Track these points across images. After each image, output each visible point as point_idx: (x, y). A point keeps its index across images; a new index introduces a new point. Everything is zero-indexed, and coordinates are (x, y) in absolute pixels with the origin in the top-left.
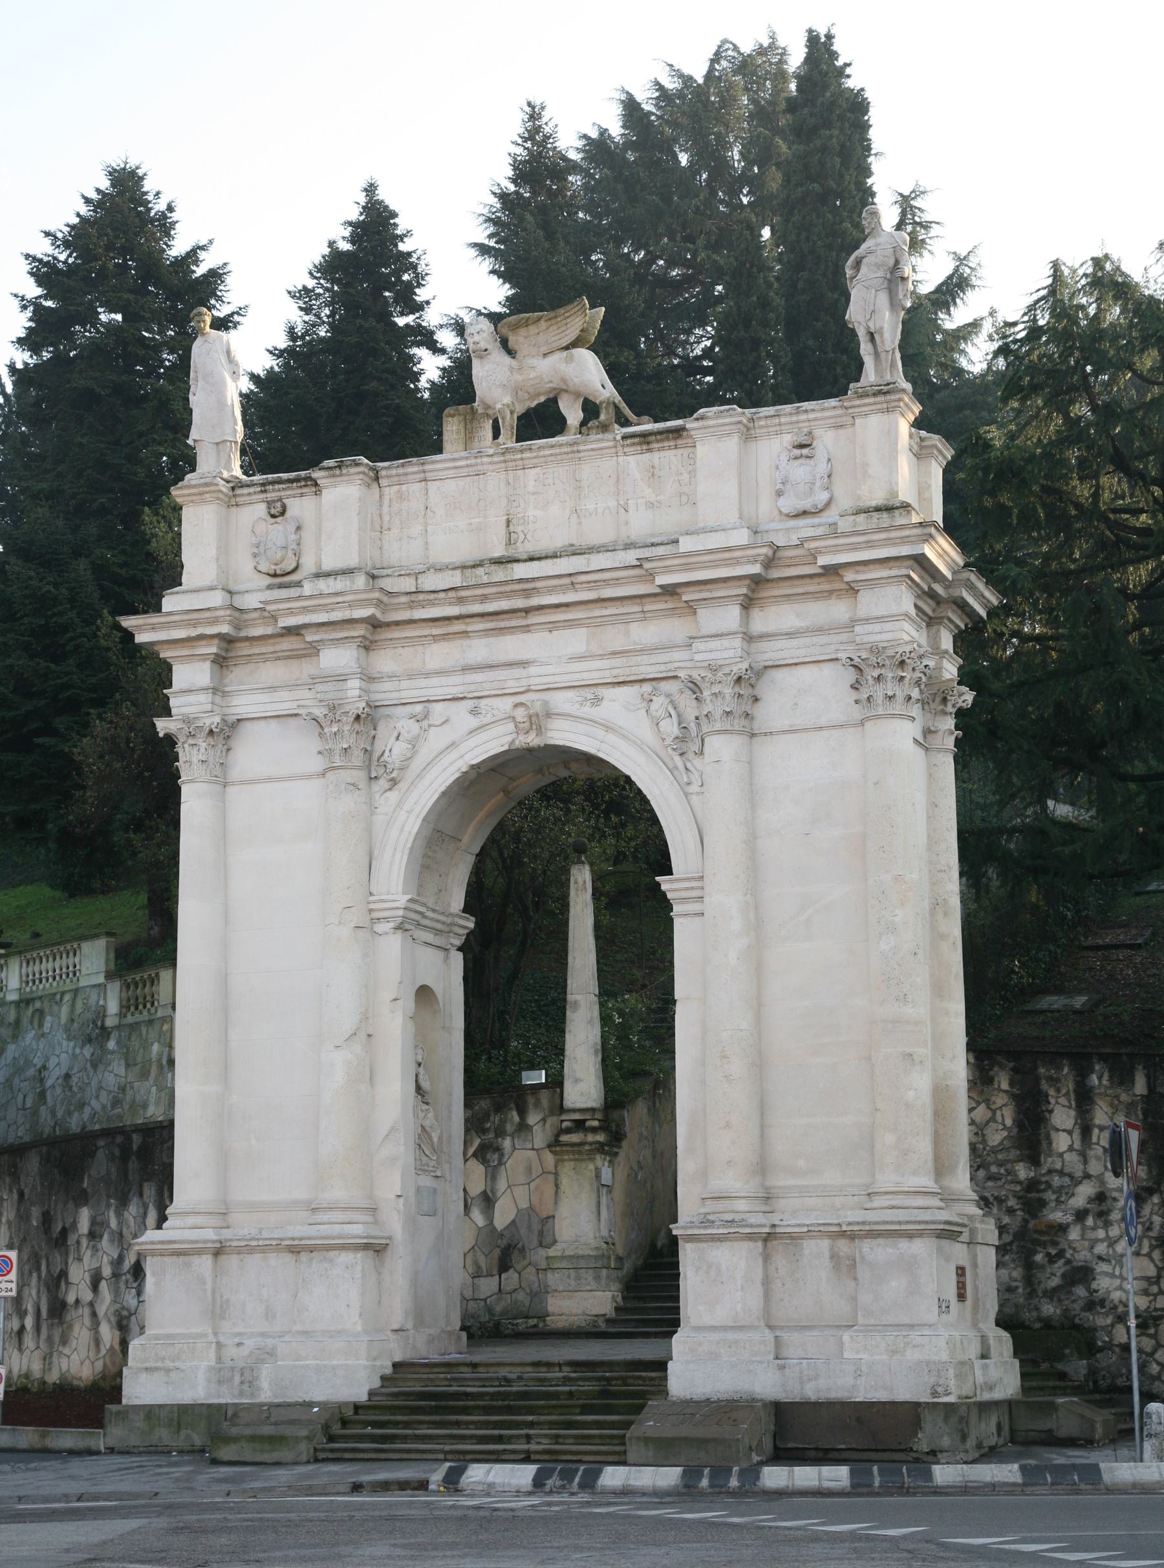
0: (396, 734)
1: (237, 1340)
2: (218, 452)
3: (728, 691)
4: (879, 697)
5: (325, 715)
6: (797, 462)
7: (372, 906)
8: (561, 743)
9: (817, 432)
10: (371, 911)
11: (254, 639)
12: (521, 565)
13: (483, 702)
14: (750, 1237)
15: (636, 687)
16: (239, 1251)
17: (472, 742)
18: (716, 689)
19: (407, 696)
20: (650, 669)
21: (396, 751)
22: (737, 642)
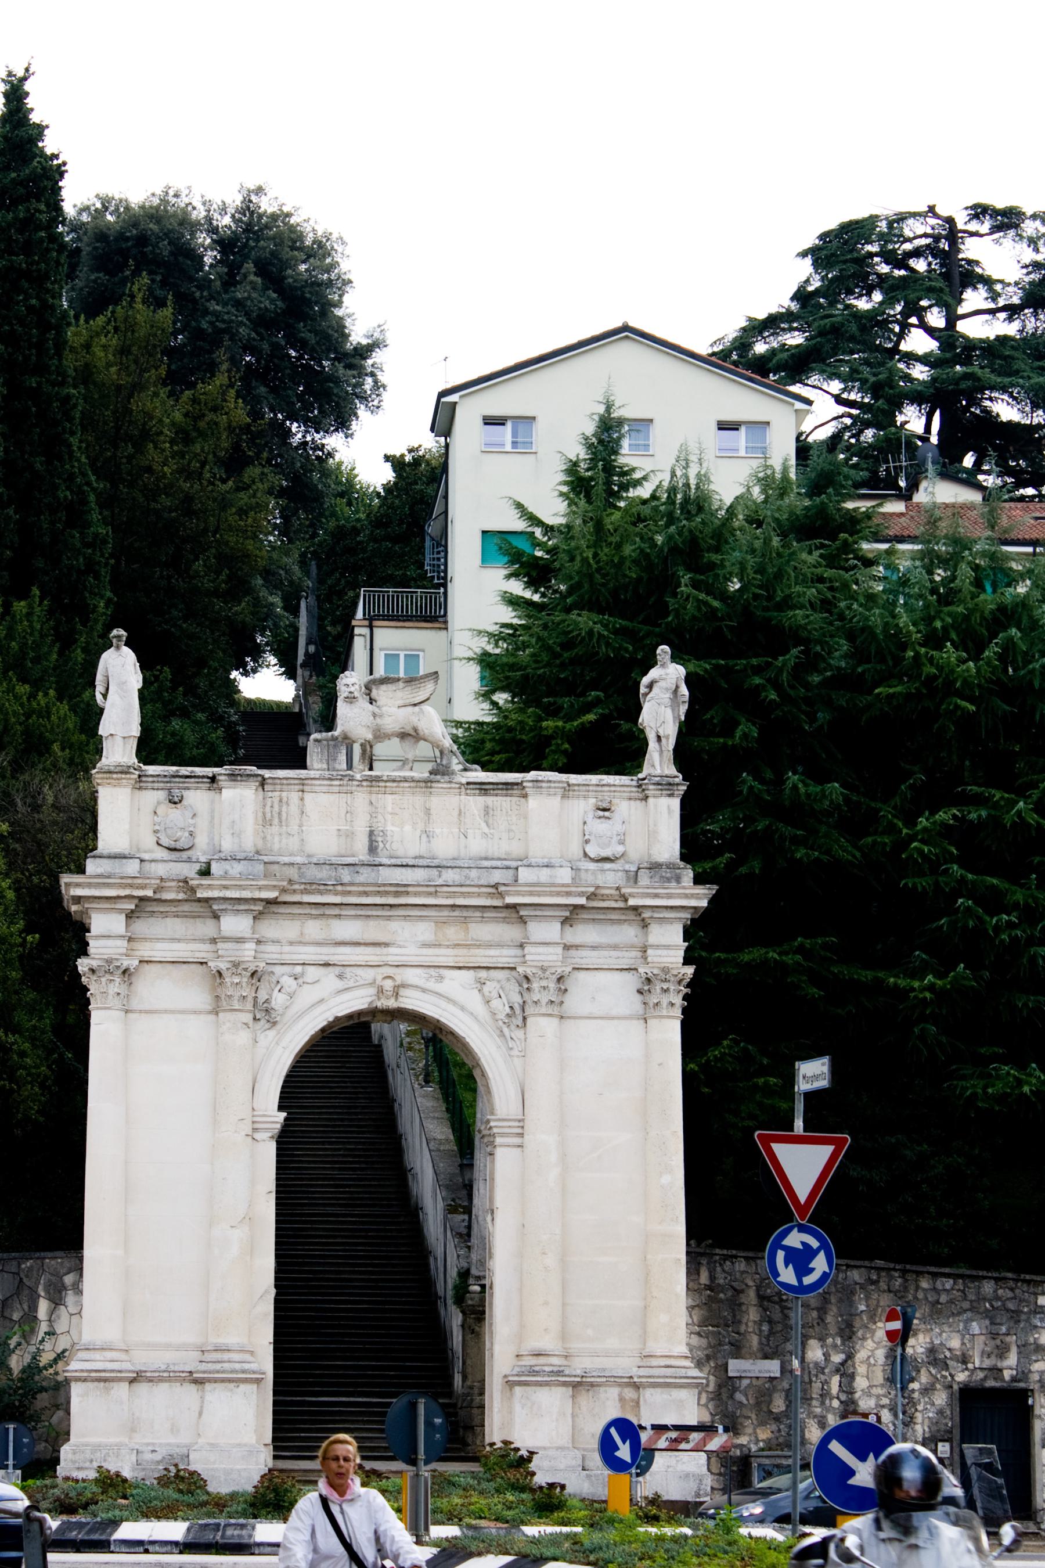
0: (279, 987)
1: (151, 1448)
2: (125, 744)
3: (552, 985)
4: (665, 1002)
5: (228, 969)
6: (599, 821)
7: (256, 1119)
8: (410, 1007)
9: (614, 801)
10: (521, 1135)
11: (166, 901)
12: (386, 868)
13: (348, 969)
14: (565, 1384)
15: (472, 972)
16: (150, 1380)
17: (339, 999)
18: (544, 983)
19: (287, 958)
20: (484, 959)
21: (279, 1000)
22: (559, 950)
